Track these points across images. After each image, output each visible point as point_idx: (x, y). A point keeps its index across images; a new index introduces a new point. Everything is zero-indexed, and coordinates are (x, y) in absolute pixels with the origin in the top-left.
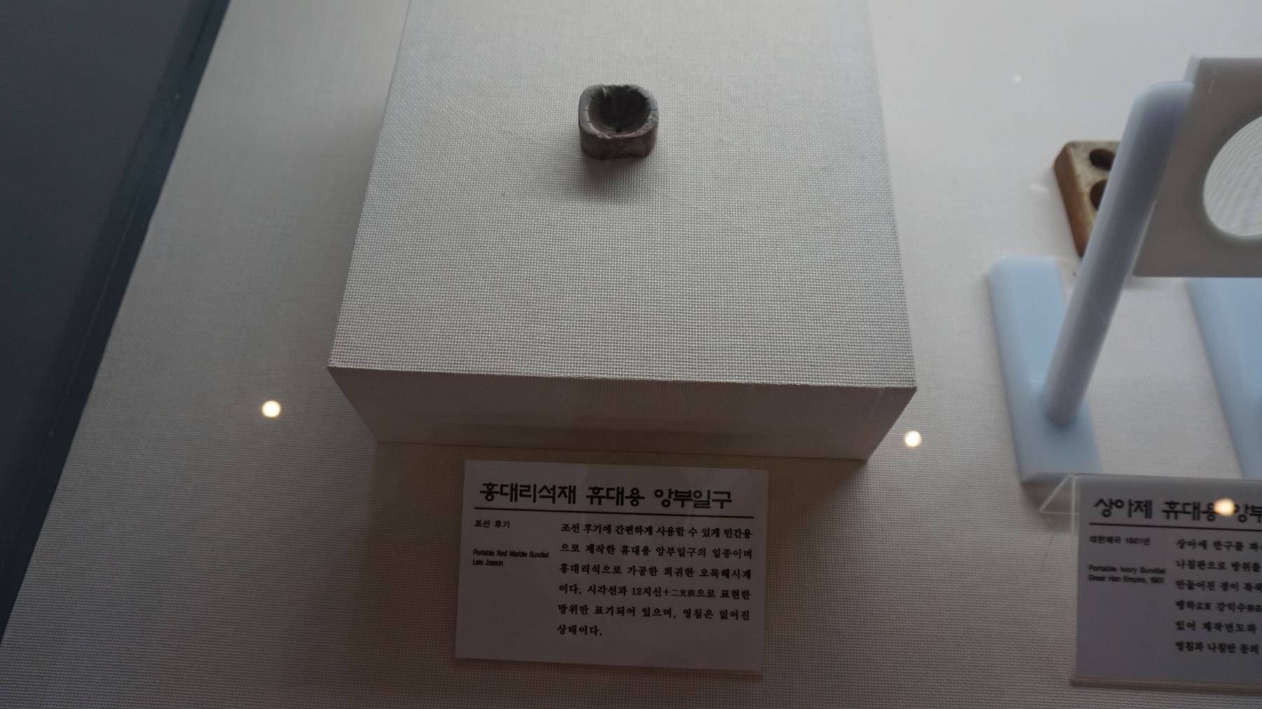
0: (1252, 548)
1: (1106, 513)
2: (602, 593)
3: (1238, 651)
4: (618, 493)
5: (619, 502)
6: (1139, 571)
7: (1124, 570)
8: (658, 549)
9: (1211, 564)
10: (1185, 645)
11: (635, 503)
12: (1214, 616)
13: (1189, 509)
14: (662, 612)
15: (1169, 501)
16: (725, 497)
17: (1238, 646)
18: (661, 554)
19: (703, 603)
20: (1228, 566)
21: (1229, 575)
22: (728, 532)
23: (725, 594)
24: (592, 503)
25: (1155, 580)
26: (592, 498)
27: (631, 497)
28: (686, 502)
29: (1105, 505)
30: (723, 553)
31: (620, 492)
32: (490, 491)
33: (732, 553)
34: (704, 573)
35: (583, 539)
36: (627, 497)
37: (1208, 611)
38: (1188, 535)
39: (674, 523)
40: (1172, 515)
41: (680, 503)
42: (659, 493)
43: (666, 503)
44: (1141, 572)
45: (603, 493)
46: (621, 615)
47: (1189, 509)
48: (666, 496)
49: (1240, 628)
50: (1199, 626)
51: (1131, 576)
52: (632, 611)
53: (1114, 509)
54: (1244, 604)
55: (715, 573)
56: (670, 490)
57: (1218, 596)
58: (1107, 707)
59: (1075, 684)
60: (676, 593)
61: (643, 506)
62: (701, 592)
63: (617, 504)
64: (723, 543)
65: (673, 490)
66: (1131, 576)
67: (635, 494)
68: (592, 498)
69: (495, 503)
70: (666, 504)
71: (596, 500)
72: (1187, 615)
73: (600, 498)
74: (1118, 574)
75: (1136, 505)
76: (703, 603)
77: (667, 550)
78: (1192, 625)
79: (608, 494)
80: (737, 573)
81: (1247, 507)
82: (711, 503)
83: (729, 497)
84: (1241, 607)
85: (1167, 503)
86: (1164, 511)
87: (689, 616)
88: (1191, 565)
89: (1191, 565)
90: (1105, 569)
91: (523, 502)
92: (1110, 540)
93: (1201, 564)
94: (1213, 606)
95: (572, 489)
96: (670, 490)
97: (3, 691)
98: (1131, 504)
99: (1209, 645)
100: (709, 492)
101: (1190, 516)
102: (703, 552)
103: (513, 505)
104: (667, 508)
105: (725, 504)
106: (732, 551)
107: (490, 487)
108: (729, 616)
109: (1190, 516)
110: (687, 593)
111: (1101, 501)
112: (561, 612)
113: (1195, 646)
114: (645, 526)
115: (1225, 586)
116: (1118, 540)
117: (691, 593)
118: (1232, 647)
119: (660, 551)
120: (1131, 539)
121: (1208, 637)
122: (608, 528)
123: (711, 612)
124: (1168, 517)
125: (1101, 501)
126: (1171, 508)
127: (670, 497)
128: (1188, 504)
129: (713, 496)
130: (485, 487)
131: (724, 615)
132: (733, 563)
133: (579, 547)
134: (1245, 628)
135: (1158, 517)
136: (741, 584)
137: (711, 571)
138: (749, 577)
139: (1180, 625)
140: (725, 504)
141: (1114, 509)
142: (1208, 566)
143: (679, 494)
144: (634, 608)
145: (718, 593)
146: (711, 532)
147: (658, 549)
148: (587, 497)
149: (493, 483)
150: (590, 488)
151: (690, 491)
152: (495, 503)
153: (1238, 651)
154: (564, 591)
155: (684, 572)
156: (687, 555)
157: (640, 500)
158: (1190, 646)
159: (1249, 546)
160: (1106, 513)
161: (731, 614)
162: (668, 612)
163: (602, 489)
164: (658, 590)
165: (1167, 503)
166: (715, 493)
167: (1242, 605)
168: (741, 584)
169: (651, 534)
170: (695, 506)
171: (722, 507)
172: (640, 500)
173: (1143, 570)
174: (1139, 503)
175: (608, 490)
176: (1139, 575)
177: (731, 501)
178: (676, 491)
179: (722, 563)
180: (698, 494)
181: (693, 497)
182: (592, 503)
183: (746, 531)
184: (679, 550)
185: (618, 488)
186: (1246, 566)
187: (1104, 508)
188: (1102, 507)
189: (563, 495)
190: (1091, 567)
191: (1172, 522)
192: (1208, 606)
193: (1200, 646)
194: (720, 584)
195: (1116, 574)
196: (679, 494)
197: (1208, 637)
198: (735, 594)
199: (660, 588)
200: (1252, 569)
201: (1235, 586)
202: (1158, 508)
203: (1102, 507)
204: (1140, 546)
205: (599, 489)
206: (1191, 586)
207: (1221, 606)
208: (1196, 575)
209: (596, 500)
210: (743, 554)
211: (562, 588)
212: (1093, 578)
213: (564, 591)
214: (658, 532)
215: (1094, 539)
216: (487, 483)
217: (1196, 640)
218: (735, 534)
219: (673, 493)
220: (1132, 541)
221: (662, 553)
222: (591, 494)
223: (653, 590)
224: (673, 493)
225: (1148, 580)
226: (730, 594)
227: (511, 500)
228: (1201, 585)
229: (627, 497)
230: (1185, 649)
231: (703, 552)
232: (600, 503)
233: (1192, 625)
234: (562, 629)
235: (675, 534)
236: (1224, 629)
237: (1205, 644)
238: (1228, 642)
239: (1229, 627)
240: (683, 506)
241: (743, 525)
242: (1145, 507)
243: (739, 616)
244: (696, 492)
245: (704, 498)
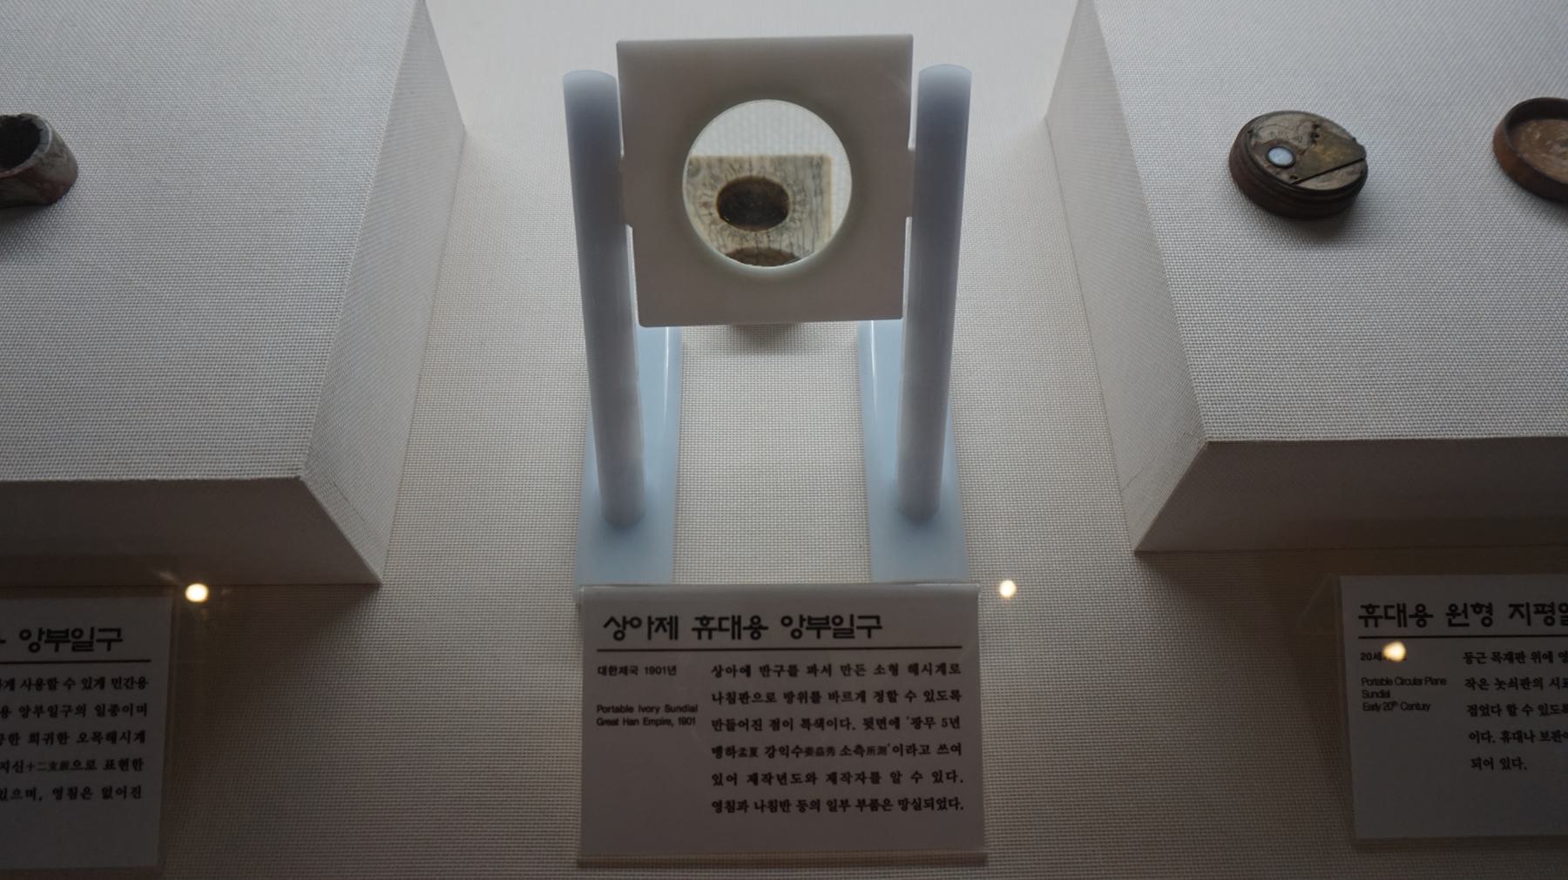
0: (809, 672)
1: (619, 636)
3: (794, 809)
4: (1399, 611)
5: (736, 635)
6: (662, 709)
7: (643, 709)
8: (21, 709)
10: (724, 805)
11: (756, 635)
12: (761, 765)
13: (727, 624)
14: (23, 794)
16: (873, 622)
17: (794, 802)
18: (25, 716)
19: (78, 779)
20: (779, 697)
21: (780, 710)
22: (765, 670)
23: (110, 765)
24: (700, 637)
25: (684, 721)
26: (699, 631)
27: (750, 628)
28: (822, 632)
30: (109, 711)
31: (1402, 610)
33: (121, 709)
34: (83, 738)
35: (1492, 671)
37: (754, 758)
38: (726, 660)
40: (705, 634)
42: (25, 634)
43: (619, 635)
44: (666, 711)
45: (1379, 612)
46: (1478, 768)
47: (1392, 612)
48: (796, 625)
49: (796, 779)
50: (822, 778)
51: (655, 717)
52: (1490, 763)
53: (629, 630)
54: (800, 746)
55: (97, 737)
56: (801, 617)
57: (767, 737)
58: (1039, 878)
59: (582, 865)
60: (42, 767)
61: (766, 639)
62: (77, 763)
64: (109, 696)
65: (805, 617)
66: (655, 717)
67: (1421, 612)
68: (699, 631)
69: (715, 643)
70: (34, 648)
71: (1371, 622)
72: (727, 765)
73: (1376, 618)
74: (636, 715)
75: (657, 623)
76: (78, 779)
78: (733, 778)
79: (720, 624)
80: (126, 736)
81: (802, 619)
82: (855, 630)
83: (878, 622)
87: (59, 797)
88: (731, 698)
89: (731, 698)
90: (618, 710)
91: (827, 637)
92: (624, 670)
93: (744, 697)
94: (761, 751)
95: (736, 620)
96: (801, 617)
98: (650, 623)
99: (756, 804)
100: (852, 616)
102: (82, 710)
103: (736, 644)
104: (1423, 629)
110: (58, 767)
111: (612, 619)
112: (57, 798)
113: (737, 806)
114: (936, 662)
115: (775, 724)
116: (635, 671)
117: (64, 766)
118: (785, 805)
119: (25, 711)
120: (652, 667)
121: (754, 794)
123: (89, 789)
125: (612, 619)
127: (801, 625)
129: (858, 622)
130: (1364, 610)
131: (107, 793)
132: (121, 723)
133: (776, 696)
134: (803, 778)
135: (687, 637)
136: (132, 750)
137: (92, 736)
138: (143, 740)
139: (717, 779)
140: (874, 632)
141: (629, 630)
143: (813, 622)
145: (100, 764)
146: (94, 683)
147: (21, 709)
148: (694, 629)
149: (1374, 604)
151: (827, 618)
152: (627, 643)
153: (794, 809)
154: (899, 753)
155: (55, 737)
156: (61, 715)
157: (762, 632)
158: (731, 807)
159: (806, 670)
160: (619, 636)
161: (117, 792)
162: (32, 793)
164: (20, 764)
166: (860, 617)
167: (797, 747)
168: (132, 750)
169: (12, 688)
170: (835, 636)
171: (869, 636)
172: (762, 632)
173: (668, 709)
174: (661, 620)
175: (721, 619)
176: (662, 715)
177: (121, 640)
179: (107, 724)
180: (837, 621)
181: (831, 625)
182: (700, 637)
183: (37, 681)
184: (50, 709)
186: (803, 696)
187: (616, 628)
188: (613, 628)
189: (661, 629)
190: (600, 708)
191: (705, 642)
192: (754, 752)
194: (104, 751)
196: (813, 622)
197: (754, 794)
198: (124, 764)
199: (22, 762)
200: (810, 700)
202: (686, 625)
203: (613, 628)
204: (665, 677)
205: (709, 619)
206: (731, 726)
207: (771, 751)
208: (738, 712)
209: (1371, 622)
210: (135, 709)
211: (1472, 736)
212: (602, 722)
213: (899, 753)
214: (22, 686)
215: (603, 671)
217: (739, 798)
218: (125, 684)
219: (805, 620)
220: (653, 670)
221: (27, 714)
222: (1365, 614)
223: (12, 764)
224: (805, 620)
226: (116, 765)
227: (733, 638)
228: (744, 724)
229: (745, 628)
230: (725, 811)
231: (82, 710)
232: (710, 637)
233: (733, 778)
235: (46, 687)
236: (775, 781)
237: (751, 804)
239: (782, 779)
240: (819, 636)
241: (137, 671)
242: (670, 625)
243: (128, 794)
244: (74, 632)
245: (86, 638)
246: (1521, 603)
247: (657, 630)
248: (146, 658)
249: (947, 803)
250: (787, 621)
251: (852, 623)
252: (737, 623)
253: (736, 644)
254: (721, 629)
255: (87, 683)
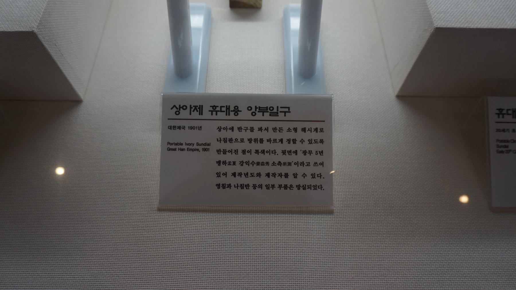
1: (177, 113)
2: (248, 165)
3: (251, 188)
6: (195, 145)
7: (187, 144)
9: (236, 140)
10: (221, 186)
12: (238, 169)
13: (224, 109)
15: (499, 108)
16: (287, 110)
17: (251, 185)
20: (246, 140)
21: (246, 146)
24: (212, 114)
25: (205, 150)
26: (212, 111)
28: (265, 113)
29: (177, 108)
31: (228, 108)
32: (500, 112)
36: (231, 111)
38: (223, 124)
39: (278, 125)
41: (262, 113)
42: (249, 108)
45: (218, 109)
48: (253, 110)
49: (252, 175)
50: (229, 174)
51: (191, 148)
56: (256, 106)
57: (241, 157)
59: (160, 210)
61: (241, 116)
63: (226, 115)
65: (258, 107)
66: (191, 148)
68: (212, 111)
70: (254, 114)
72: (223, 169)
74: (184, 147)
75: (194, 108)
77: (308, 152)
78: (225, 174)
79: (221, 109)
81: (256, 108)
82: (279, 113)
83: (289, 110)
84: (253, 163)
85: (497, 109)
86: (497, 114)
88: (225, 140)
89: (225, 140)
90: (176, 144)
91: (267, 116)
92: (179, 128)
93: (231, 140)
96: (256, 106)
97: (1, 240)
98: (191, 108)
100: (278, 107)
101: (511, 116)
103: (228, 117)
105: (287, 113)
106: (227, 150)
107: (214, 108)
108: (221, 175)
109: (511, 116)
111: (175, 106)
116: (184, 128)
118: (247, 186)
121: (234, 181)
122: (232, 129)
124: (499, 117)
125: (175, 106)
126: (500, 112)
127: (256, 110)
128: (510, 110)
129: (280, 110)
130: (212, 108)
134: (255, 175)
135: (206, 114)
139: (218, 175)
142: (234, 141)
144: (226, 173)
148: (209, 111)
149: (216, 105)
150: (211, 106)
151: (267, 107)
158: (224, 186)
160: (177, 113)
163: (218, 107)
165: (497, 109)
166: (281, 108)
170: (270, 115)
171: (285, 116)
173: (198, 144)
174: (196, 107)
175: (221, 107)
176: (195, 147)
177: (290, 112)
178: (259, 107)
180: (271, 109)
181: (269, 110)
182: (212, 114)
185: (227, 106)
186: (256, 140)
187: (176, 110)
188: (175, 110)
189: (195, 111)
190: (169, 143)
191: (214, 117)
192: (234, 163)
193: (229, 186)
195: (182, 147)
197: (234, 181)
201: (250, 152)
202: (206, 109)
203: (175, 110)
204: (196, 131)
205: (216, 107)
206: (225, 152)
208: (228, 146)
212: (169, 149)
215: (170, 128)
216: (213, 105)
219: (257, 108)
220: (192, 128)
222: (212, 110)
224: (257, 108)
225: (201, 149)
228: (230, 151)
229: (231, 111)
230: (221, 188)
232: (216, 114)
233: (225, 174)
234: (218, 186)
236: (243, 176)
237: (232, 185)
238: (245, 183)
240: (263, 115)
242: (200, 109)
245: (275, 110)
246: (197, 105)
247: (193, 111)
248: (324, 120)
249: (317, 187)
250: (250, 108)
251: (278, 110)
252: (228, 109)
253: (228, 117)
254: (221, 111)
255: (275, 129)
